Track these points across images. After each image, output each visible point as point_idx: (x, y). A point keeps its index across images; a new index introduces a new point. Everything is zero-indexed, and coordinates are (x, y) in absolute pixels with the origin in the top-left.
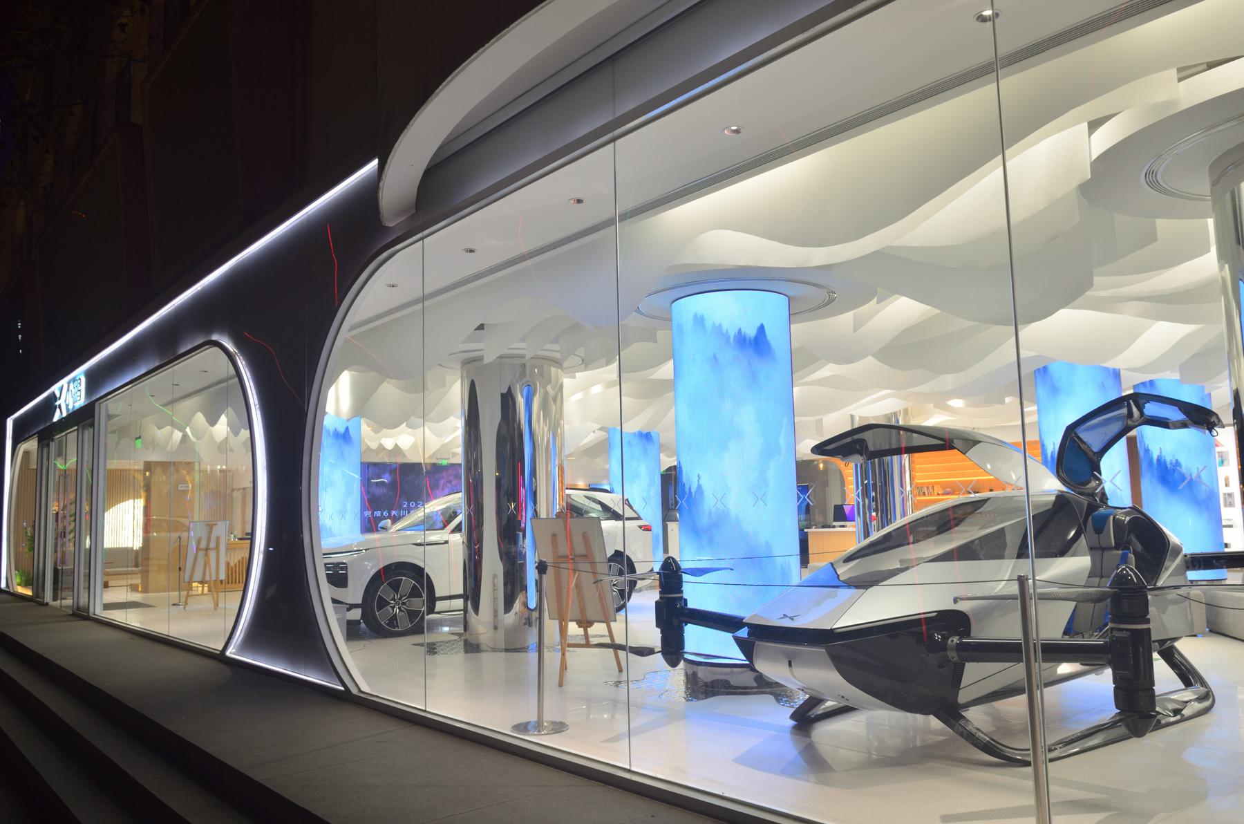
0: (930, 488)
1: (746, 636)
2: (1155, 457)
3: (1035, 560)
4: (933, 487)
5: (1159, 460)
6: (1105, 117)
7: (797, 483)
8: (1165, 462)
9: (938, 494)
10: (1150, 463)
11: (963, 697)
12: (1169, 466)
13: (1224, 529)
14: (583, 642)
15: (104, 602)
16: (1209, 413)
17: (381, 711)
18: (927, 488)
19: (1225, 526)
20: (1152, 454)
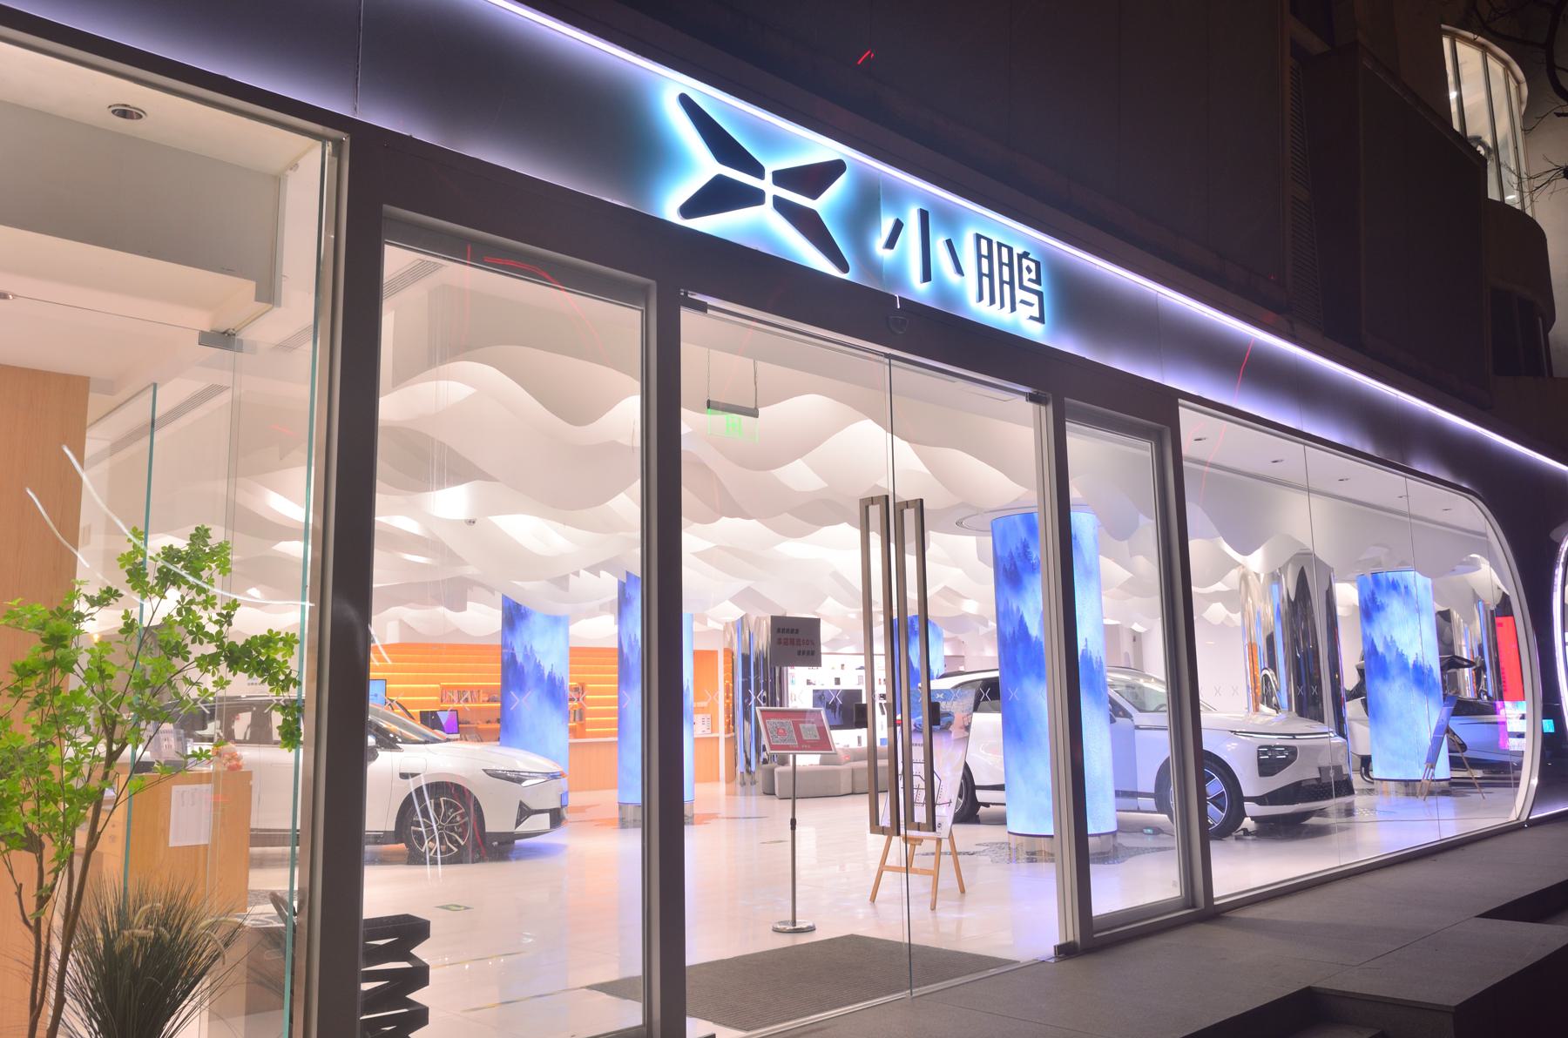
0: (475, 693)
1: (364, 918)
2: (546, 674)
3: (863, 687)
4: (479, 691)
5: (549, 676)
6: (1487, 917)
7: (1440, 654)
8: (555, 678)
9: (483, 701)
10: (540, 679)
11: (1417, 573)
12: (1095, 666)
13: (998, 667)
14: (930, 879)
15: (695, 649)
16: (47, 651)
17: (1339, 879)
18: (472, 692)
19: (997, 670)
20: (1407, 659)
